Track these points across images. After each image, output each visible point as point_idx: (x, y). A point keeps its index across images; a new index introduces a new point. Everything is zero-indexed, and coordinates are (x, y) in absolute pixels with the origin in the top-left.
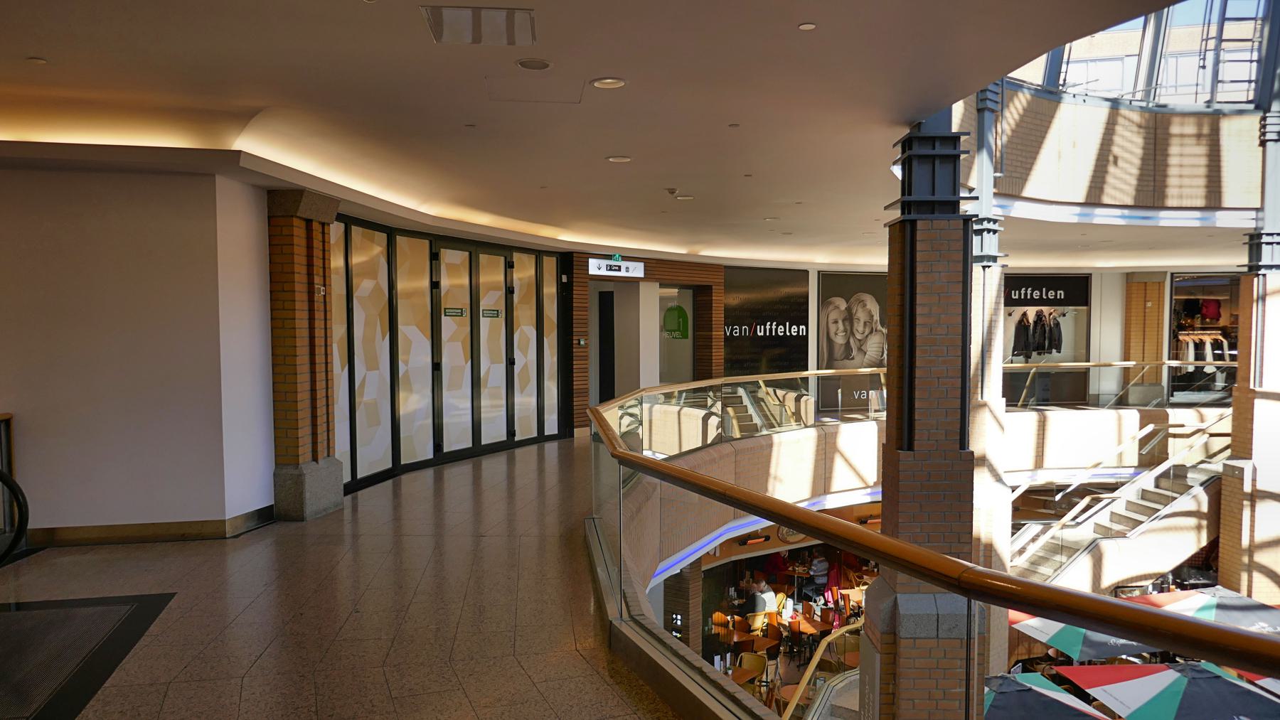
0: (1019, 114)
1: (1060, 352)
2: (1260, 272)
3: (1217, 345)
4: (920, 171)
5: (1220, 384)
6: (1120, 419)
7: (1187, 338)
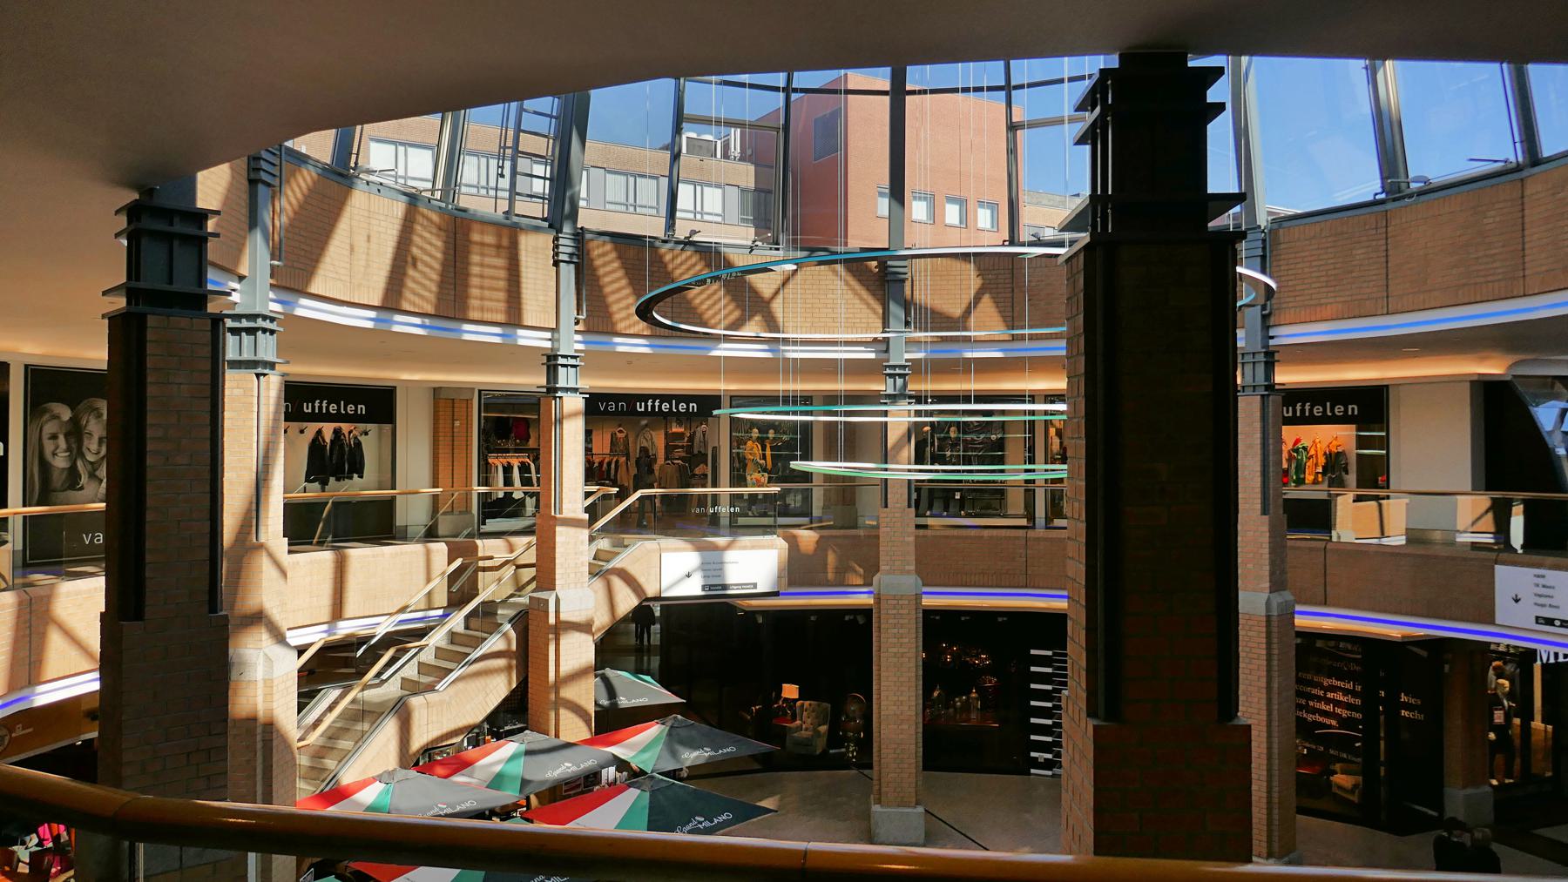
0: (303, 195)
2: (557, 395)
3: (524, 468)
7: (496, 461)
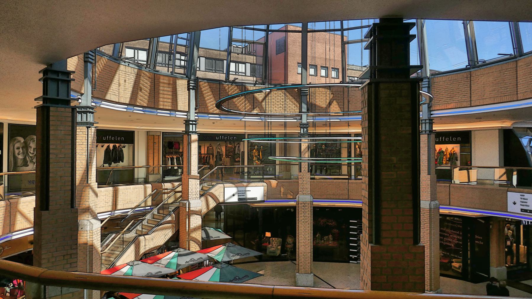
7: (169, 157)
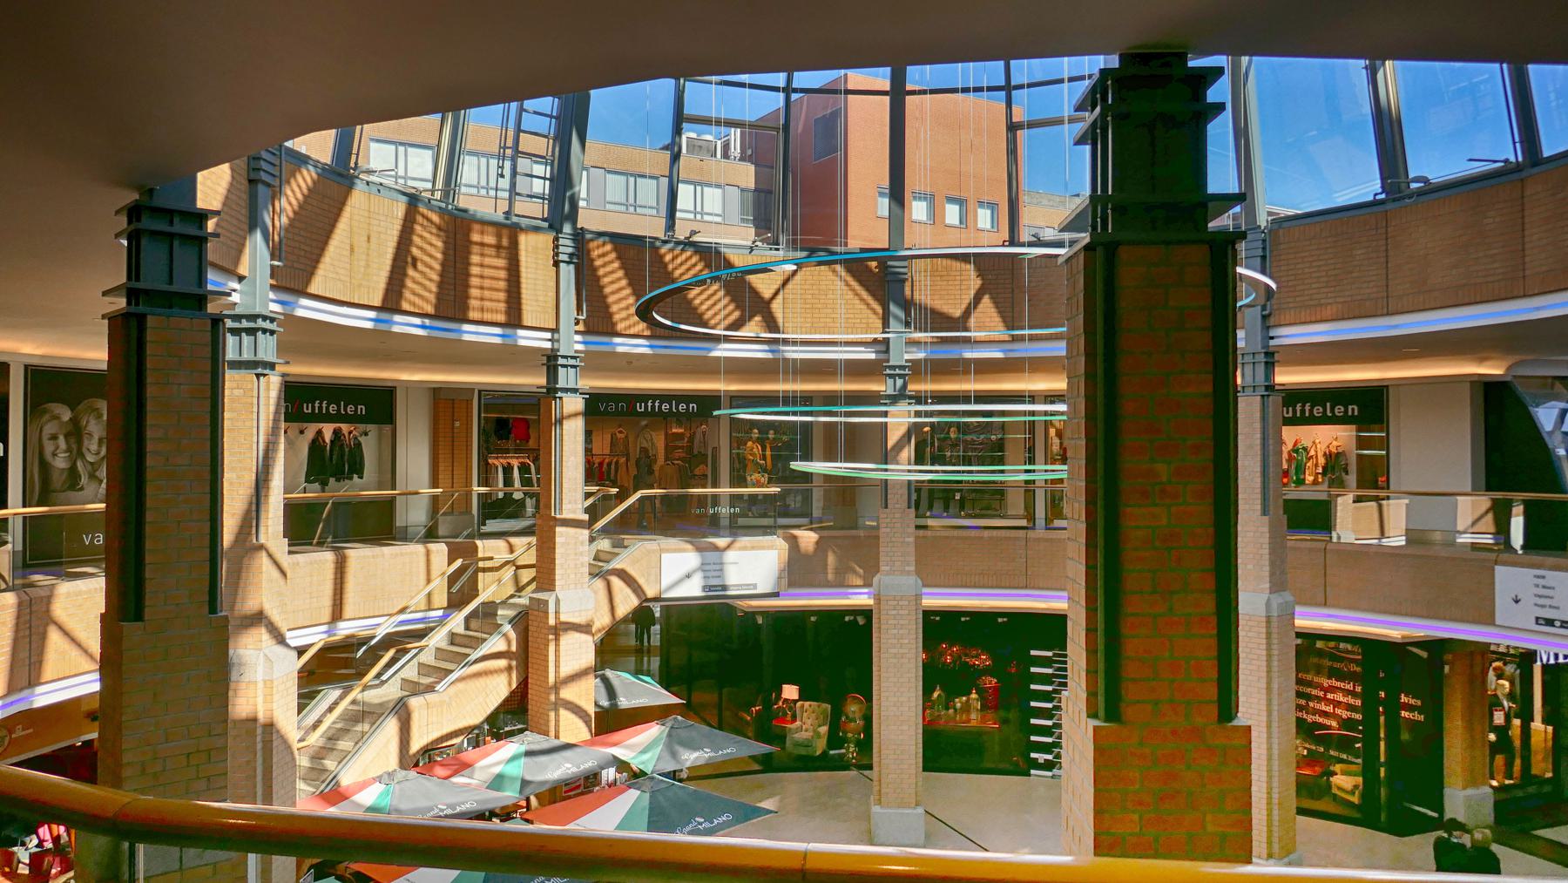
0: (303, 195)
1: (361, 478)
2: (557, 395)
3: (524, 469)
4: (153, 253)
5: (530, 510)
6: (428, 553)
7: (496, 462)
